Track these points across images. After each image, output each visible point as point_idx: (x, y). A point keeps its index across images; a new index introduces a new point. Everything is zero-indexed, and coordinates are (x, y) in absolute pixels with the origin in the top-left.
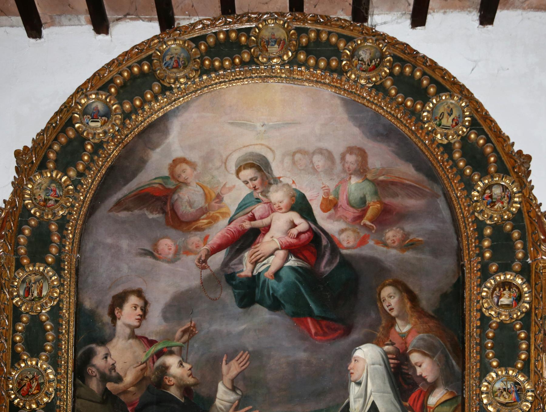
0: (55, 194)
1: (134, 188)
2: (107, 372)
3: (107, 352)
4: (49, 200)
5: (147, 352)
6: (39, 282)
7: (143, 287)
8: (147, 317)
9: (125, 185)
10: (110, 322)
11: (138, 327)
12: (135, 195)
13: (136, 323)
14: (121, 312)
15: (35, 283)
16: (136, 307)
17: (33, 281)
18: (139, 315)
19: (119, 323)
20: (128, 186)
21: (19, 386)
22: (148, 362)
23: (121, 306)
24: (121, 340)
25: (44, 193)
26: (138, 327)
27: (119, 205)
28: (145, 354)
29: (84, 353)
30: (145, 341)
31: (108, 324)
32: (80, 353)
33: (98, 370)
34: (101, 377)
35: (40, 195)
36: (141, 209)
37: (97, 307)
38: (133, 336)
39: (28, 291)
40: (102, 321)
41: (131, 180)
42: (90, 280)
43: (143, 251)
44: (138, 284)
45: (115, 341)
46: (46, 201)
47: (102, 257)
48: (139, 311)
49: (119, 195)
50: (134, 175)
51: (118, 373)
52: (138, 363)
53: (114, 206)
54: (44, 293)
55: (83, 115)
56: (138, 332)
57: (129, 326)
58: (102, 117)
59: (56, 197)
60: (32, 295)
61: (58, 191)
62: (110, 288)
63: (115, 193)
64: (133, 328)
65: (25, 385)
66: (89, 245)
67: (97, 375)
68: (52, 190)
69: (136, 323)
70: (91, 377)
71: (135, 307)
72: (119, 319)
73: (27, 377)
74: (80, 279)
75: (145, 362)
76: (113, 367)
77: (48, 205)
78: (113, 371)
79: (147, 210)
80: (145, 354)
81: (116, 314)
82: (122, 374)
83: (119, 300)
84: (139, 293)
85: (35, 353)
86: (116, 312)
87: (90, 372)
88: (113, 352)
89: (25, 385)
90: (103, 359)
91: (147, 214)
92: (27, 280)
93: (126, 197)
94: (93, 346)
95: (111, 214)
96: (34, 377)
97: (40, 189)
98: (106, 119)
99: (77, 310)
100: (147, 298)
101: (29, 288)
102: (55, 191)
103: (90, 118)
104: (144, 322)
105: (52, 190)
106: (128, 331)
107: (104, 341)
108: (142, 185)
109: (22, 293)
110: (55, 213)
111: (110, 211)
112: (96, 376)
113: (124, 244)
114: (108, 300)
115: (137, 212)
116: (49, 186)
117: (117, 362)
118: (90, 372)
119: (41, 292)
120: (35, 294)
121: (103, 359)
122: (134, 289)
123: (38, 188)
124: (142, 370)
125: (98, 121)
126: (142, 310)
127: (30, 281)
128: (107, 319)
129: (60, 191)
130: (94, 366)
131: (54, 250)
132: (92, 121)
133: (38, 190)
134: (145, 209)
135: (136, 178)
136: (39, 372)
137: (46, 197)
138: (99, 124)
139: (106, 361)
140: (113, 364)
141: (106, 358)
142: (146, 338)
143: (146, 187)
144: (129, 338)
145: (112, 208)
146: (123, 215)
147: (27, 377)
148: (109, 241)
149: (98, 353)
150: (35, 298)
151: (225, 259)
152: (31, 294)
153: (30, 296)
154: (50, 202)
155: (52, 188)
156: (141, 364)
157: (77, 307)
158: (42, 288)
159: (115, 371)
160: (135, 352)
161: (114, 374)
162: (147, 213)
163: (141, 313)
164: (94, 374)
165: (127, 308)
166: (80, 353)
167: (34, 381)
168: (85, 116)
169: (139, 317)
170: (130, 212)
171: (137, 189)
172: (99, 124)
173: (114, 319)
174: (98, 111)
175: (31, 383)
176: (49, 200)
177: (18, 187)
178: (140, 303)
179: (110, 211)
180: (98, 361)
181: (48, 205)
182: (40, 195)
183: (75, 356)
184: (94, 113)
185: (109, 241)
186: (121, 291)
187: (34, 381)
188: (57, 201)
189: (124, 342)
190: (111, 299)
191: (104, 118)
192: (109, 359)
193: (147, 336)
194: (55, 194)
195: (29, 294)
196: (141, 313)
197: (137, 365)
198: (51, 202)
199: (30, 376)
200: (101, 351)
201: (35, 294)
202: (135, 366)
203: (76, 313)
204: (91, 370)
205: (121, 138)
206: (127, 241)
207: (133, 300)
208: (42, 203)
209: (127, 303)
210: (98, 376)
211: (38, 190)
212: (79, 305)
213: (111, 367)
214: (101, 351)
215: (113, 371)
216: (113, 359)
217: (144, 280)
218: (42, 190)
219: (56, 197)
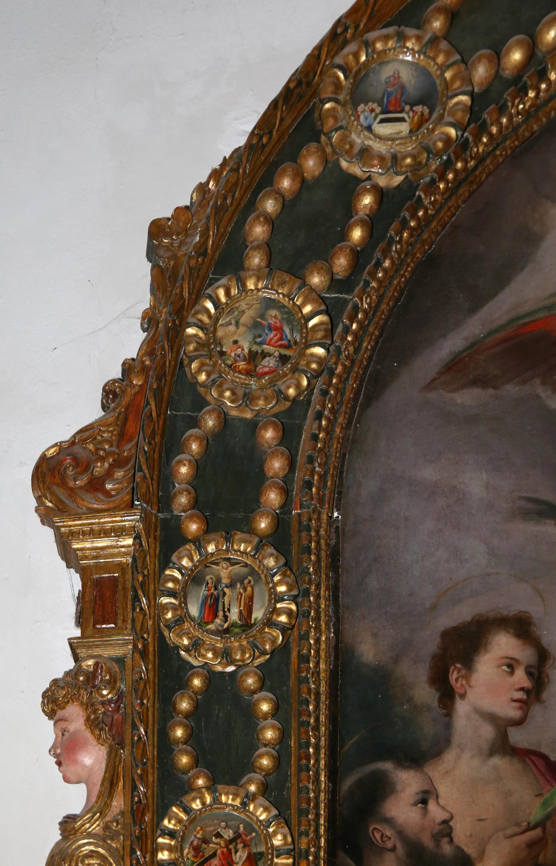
0: (281, 339)
1: (503, 321)
2: (427, 841)
3: (426, 787)
4: (264, 355)
5: (547, 795)
6: (242, 583)
7: (534, 609)
8: (545, 695)
9: (474, 309)
10: (436, 704)
11: (519, 723)
12: (506, 340)
13: (513, 712)
14: (467, 678)
15: (231, 585)
16: (511, 666)
17: (225, 581)
18: (522, 689)
19: (462, 708)
20: (484, 312)
21: (195, 857)
22: (548, 824)
23: (468, 662)
24: (466, 756)
25: (250, 337)
26: (519, 723)
27: (458, 370)
28: (538, 802)
29: (360, 783)
30: (541, 763)
31: (429, 709)
32: (348, 783)
33: (400, 833)
34: (409, 854)
35: (236, 342)
36: (524, 382)
37: (396, 660)
38: (502, 746)
39: (213, 606)
40: (410, 700)
41: (492, 296)
42: (373, 583)
43: (531, 506)
44: (518, 599)
45: (449, 757)
46: (253, 357)
47: (406, 519)
48: (520, 677)
49: (452, 344)
50: (502, 281)
51: (459, 848)
52: (518, 824)
53: (441, 373)
54: (258, 614)
55: (355, 106)
56: (518, 737)
57: (491, 718)
58: (412, 105)
59: (281, 346)
60: (226, 618)
61: (287, 330)
62: (434, 607)
63: (444, 336)
64: (502, 726)
65: (214, 855)
66: (366, 484)
67: (399, 846)
68: (271, 328)
69: (513, 712)
70: (381, 851)
71: (510, 666)
72: (463, 696)
73: (218, 835)
74: (343, 579)
75: (541, 824)
76: (445, 830)
77: (259, 369)
78: (446, 840)
79: (544, 383)
80: (538, 802)
81: (453, 682)
82: (471, 850)
83: (463, 644)
84: (522, 627)
85: (227, 770)
86: (453, 676)
87: (378, 836)
88: (443, 789)
89: (214, 855)
90: (415, 804)
91: (543, 395)
92: (208, 578)
93: (474, 348)
94: (387, 766)
95: (432, 395)
96: (237, 836)
97: (237, 324)
98: (426, 110)
99: (336, 666)
100: (545, 642)
101: (217, 600)
102: (280, 329)
103: (378, 110)
104: (536, 710)
105: (271, 328)
106: (488, 732)
107: (417, 757)
108: (527, 308)
109: (194, 610)
110: (280, 391)
111: (429, 387)
112: (393, 849)
113: (475, 483)
114: (429, 642)
115: (511, 390)
116: (262, 316)
117: (456, 818)
118: (378, 836)
119: (250, 610)
120: (234, 615)
121: (415, 804)
122: (505, 613)
123: (229, 324)
124: (531, 845)
125: (402, 120)
126: (529, 674)
127: (219, 580)
128: (425, 694)
129: (292, 330)
130: (389, 821)
131: (273, 497)
132: (382, 121)
133: (232, 328)
134: (537, 381)
135: (507, 291)
136: (249, 828)
137: (255, 348)
138: (404, 128)
139: (425, 810)
140: (445, 822)
141: (424, 802)
142: (544, 757)
143: (541, 315)
144: (492, 753)
145: (434, 380)
146: (467, 398)
147: (218, 835)
148: (429, 473)
149: (399, 787)
150: (234, 625)
151: (77, 609)
152: (221, 613)
153: (218, 621)
154: (265, 362)
155: (272, 321)
156: (529, 828)
157: (336, 658)
158: (251, 598)
159: (451, 841)
160: (509, 793)
161: (447, 849)
162: (543, 392)
163: (527, 683)
164: (389, 845)
165: (487, 666)
166: (348, 783)
167: (240, 846)
168: (361, 108)
169: (520, 695)
170: (491, 391)
171: (511, 322)
172: (404, 128)
173: (448, 696)
174: (403, 88)
175: (229, 851)
176: (264, 355)
177: (165, 323)
178: (523, 653)
179: (429, 387)
180: (401, 809)
181: (259, 369)
182: (236, 342)
183: (333, 793)
184: (390, 94)
185: (429, 473)
186: (469, 619)
187: (240, 846)
188: (284, 359)
189: (476, 762)
190: (438, 640)
191: (419, 108)
192: (432, 806)
193: (545, 750)
194: (281, 339)
195: (216, 616)
196: (527, 683)
197: (516, 829)
198: (269, 363)
199: (229, 834)
200: (408, 782)
201: (234, 615)
202: (509, 832)
203: (333, 676)
204: (378, 832)
205: (465, 168)
206: (484, 476)
207: (504, 644)
208: (242, 365)
209: (486, 651)
210: (400, 849)
211: (232, 328)
212: (341, 653)
213: (437, 828)
214: (408, 782)
215: (446, 840)
216: (443, 808)
217: (536, 590)
218: (242, 329)
219: (281, 346)
